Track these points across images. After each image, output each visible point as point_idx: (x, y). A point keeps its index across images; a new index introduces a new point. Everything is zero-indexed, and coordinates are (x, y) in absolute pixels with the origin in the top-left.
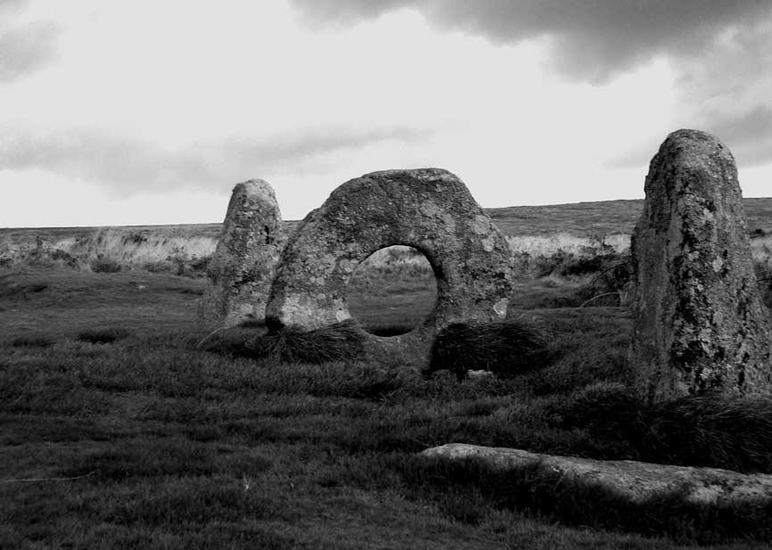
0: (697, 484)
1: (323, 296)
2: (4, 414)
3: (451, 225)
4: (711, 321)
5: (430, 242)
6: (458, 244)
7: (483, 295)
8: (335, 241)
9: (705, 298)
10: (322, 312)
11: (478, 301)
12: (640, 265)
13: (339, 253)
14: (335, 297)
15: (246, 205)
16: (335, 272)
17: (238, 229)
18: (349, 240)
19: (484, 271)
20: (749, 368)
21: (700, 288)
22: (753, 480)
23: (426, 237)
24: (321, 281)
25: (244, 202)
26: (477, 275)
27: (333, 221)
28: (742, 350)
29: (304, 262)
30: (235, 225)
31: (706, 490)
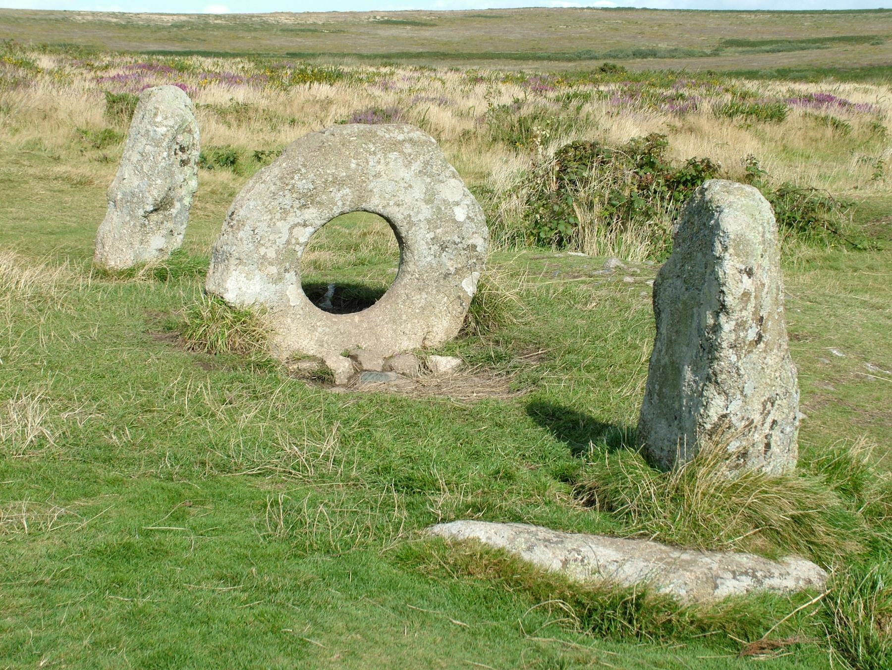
0: (725, 576)
1: (273, 270)
2: (23, 512)
3: (418, 191)
4: (742, 392)
5: (397, 209)
6: (426, 212)
7: (452, 270)
8: (288, 207)
9: (738, 369)
10: (273, 287)
11: (447, 276)
12: (663, 315)
13: (292, 219)
14: (286, 270)
15: (159, 119)
16: (288, 242)
17: (148, 147)
18: (304, 206)
19: (455, 243)
20: (776, 436)
21: (734, 358)
22: (783, 571)
23: (391, 203)
24: (271, 254)
25: (156, 115)
26: (446, 247)
27: (287, 185)
28: (769, 420)
29: (253, 231)
30: (145, 142)
31: (735, 582)
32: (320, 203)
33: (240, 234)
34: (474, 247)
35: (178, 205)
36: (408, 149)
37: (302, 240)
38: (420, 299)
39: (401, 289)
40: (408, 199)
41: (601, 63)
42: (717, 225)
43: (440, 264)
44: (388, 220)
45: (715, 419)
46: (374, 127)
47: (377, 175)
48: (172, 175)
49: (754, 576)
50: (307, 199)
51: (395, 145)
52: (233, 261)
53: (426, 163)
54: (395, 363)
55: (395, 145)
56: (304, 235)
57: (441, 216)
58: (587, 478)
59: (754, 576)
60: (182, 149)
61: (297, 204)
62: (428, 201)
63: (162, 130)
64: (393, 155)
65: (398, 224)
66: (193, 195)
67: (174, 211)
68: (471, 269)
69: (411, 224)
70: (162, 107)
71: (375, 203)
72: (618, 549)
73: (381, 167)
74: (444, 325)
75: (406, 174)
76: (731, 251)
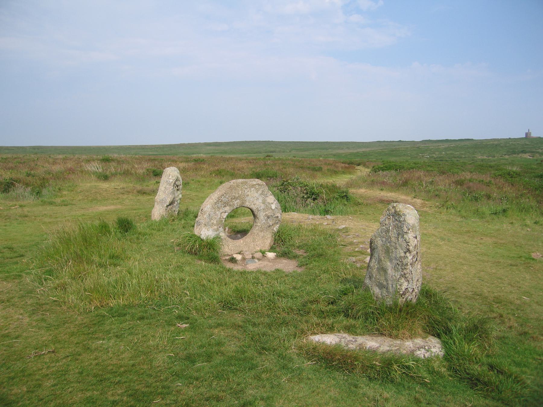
1: (216, 227)
3: (260, 200)
6: (263, 206)
13: (221, 211)
15: (170, 177)
16: (220, 218)
18: (225, 206)
21: (411, 268)
24: (215, 222)
32: (230, 205)
33: (205, 216)
34: (278, 217)
35: (176, 203)
36: (257, 187)
37: (224, 217)
38: (262, 234)
39: (255, 230)
40: (257, 203)
41: (266, 154)
42: (405, 221)
43: (268, 223)
44: (251, 209)
45: (404, 290)
46: (247, 180)
47: (248, 196)
48: (174, 194)
49: (425, 348)
50: (226, 204)
51: (253, 186)
52: (203, 225)
53: (263, 191)
54: (255, 255)
55: (253, 186)
56: (225, 215)
57: (268, 206)
58: (113, 164)
59: (425, 348)
60: (177, 186)
61: (223, 206)
62: (263, 203)
63: (171, 181)
64: (252, 189)
65: (254, 211)
66: (180, 199)
67: (175, 205)
68: (277, 223)
69: (258, 210)
70: (171, 174)
71: (247, 204)
72: (376, 341)
73: (249, 193)
74: (268, 241)
75: (256, 195)
76: (411, 230)
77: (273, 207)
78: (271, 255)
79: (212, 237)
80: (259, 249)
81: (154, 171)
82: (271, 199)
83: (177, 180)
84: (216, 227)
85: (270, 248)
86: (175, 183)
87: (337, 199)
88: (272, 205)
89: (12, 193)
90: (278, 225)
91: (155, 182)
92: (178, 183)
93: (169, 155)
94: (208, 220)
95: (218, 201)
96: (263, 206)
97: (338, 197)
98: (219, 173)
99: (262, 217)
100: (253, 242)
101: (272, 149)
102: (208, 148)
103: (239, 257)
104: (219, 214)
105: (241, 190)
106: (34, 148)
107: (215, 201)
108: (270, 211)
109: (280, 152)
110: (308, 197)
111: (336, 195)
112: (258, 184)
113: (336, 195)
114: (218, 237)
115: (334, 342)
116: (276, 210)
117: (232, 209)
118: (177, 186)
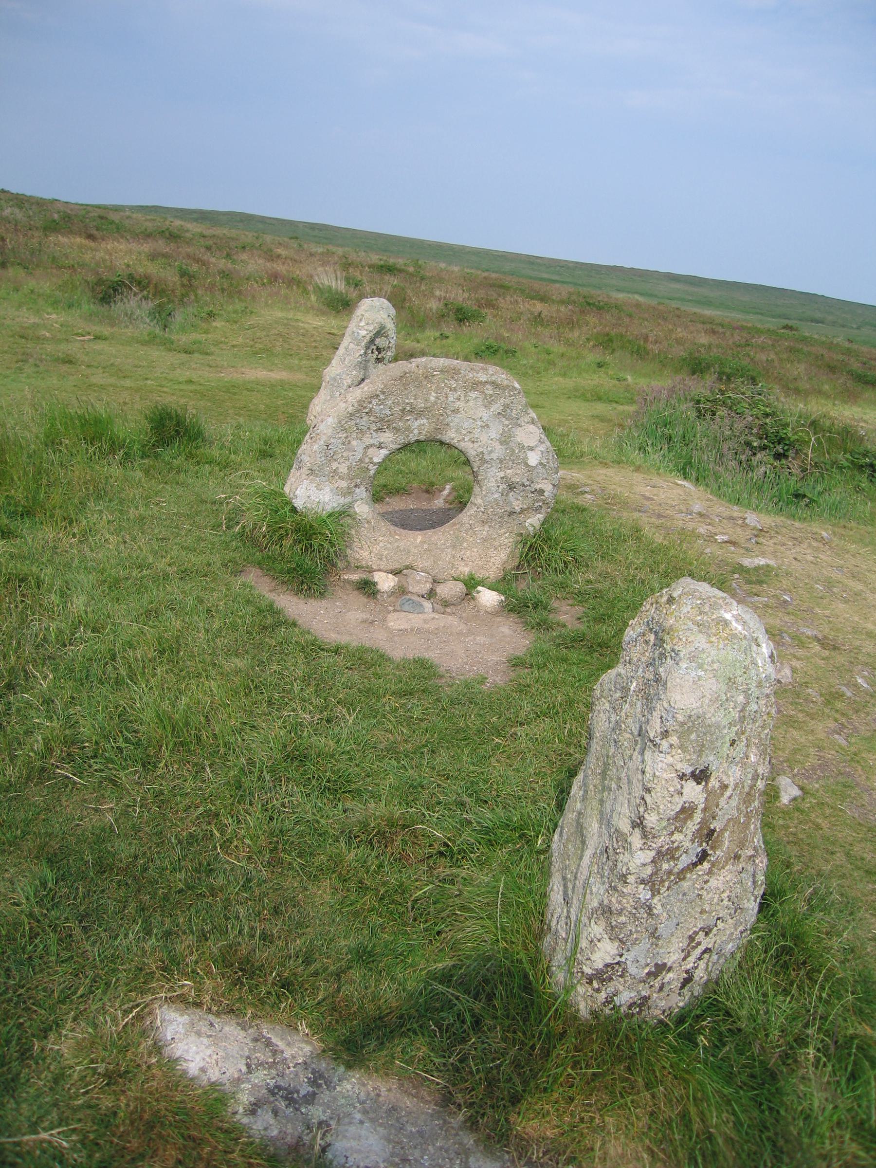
1: (344, 484)
3: (495, 432)
6: (499, 451)
13: (368, 441)
15: (362, 324)
16: (361, 461)
24: (343, 469)
32: (397, 430)
33: (315, 447)
37: (376, 460)
38: (484, 531)
40: (484, 438)
47: (456, 411)
50: (384, 424)
51: (476, 385)
53: (506, 406)
55: (476, 385)
57: (514, 455)
61: (373, 427)
62: (502, 443)
64: (473, 395)
68: (538, 510)
69: (483, 461)
70: (367, 315)
71: (451, 436)
76: (674, 739)
77: (533, 459)
78: (488, 598)
79: (329, 509)
80: (466, 570)
81: (459, 310)
82: (529, 434)
83: (380, 332)
84: (344, 484)
85: (501, 575)
86: (372, 341)
87: (841, 468)
88: (530, 454)
89: (118, 307)
90: (541, 516)
91: (438, 334)
92: (381, 342)
93: (584, 285)
94: (320, 459)
95: (358, 411)
96: (499, 451)
97: (846, 464)
98: (606, 342)
99: (491, 484)
100: (454, 547)
101: (818, 315)
102: (674, 286)
103: (385, 582)
104: (360, 450)
105: (438, 390)
106: (313, 226)
107: (350, 409)
108: (521, 469)
109: (834, 324)
110: (764, 448)
111: (842, 458)
112: (493, 383)
113: (842, 458)
114: (342, 514)
115: (214, 1075)
116: (541, 470)
117: (402, 440)
118: (378, 349)
